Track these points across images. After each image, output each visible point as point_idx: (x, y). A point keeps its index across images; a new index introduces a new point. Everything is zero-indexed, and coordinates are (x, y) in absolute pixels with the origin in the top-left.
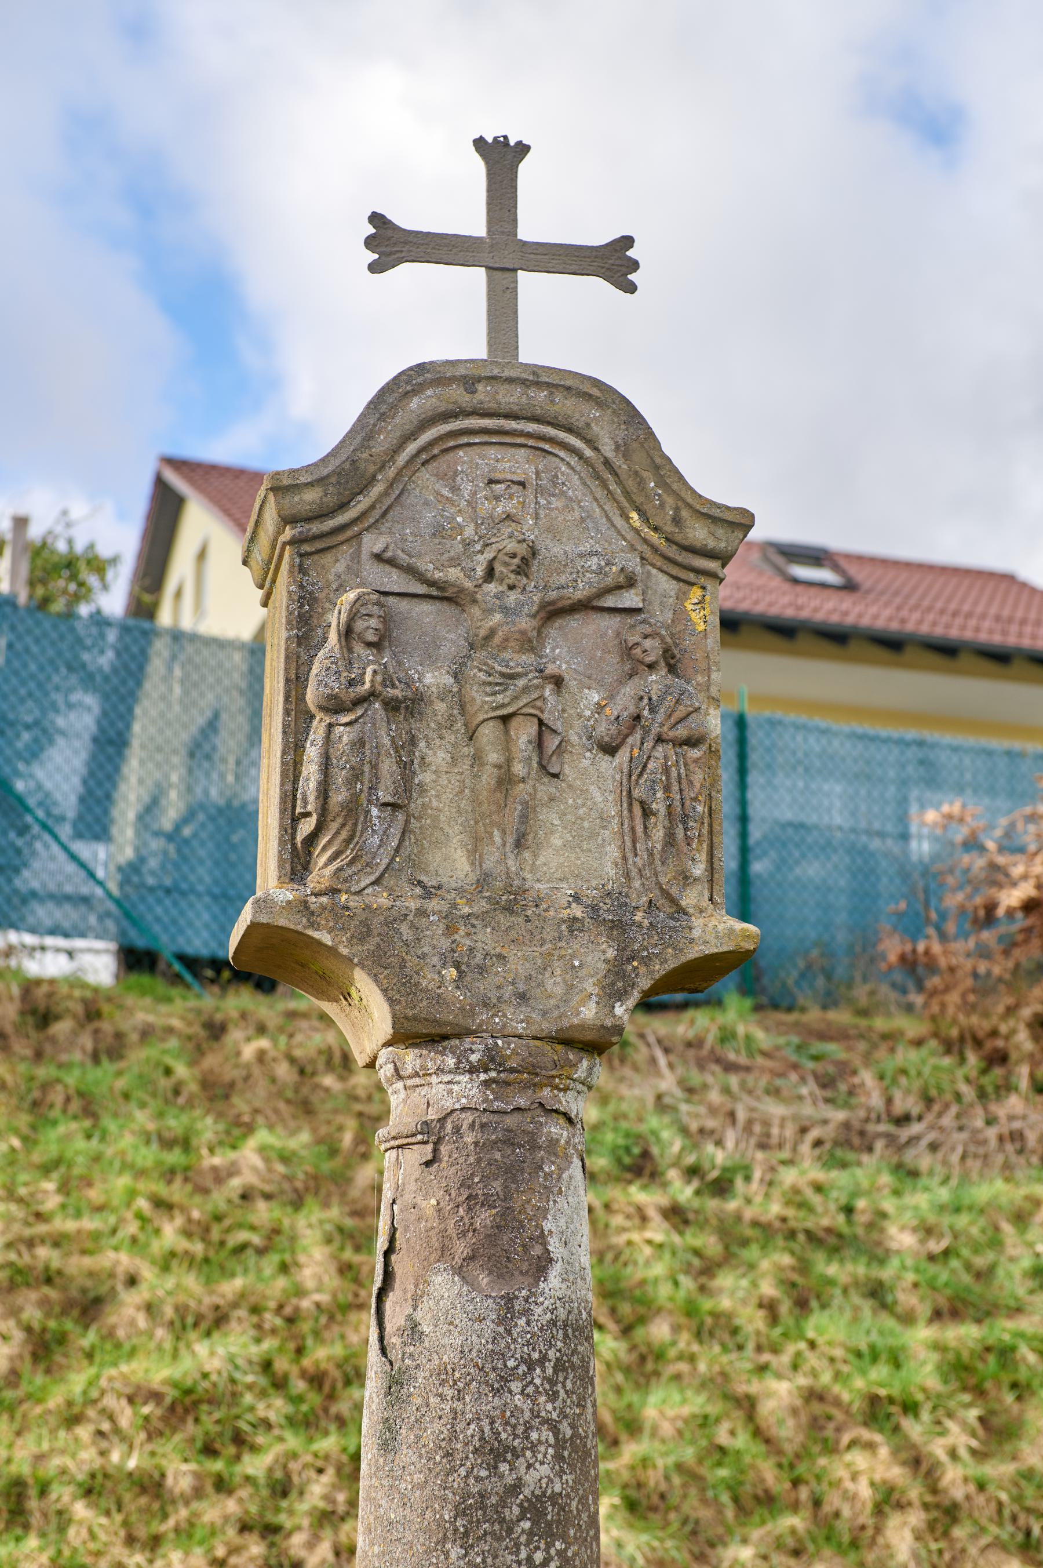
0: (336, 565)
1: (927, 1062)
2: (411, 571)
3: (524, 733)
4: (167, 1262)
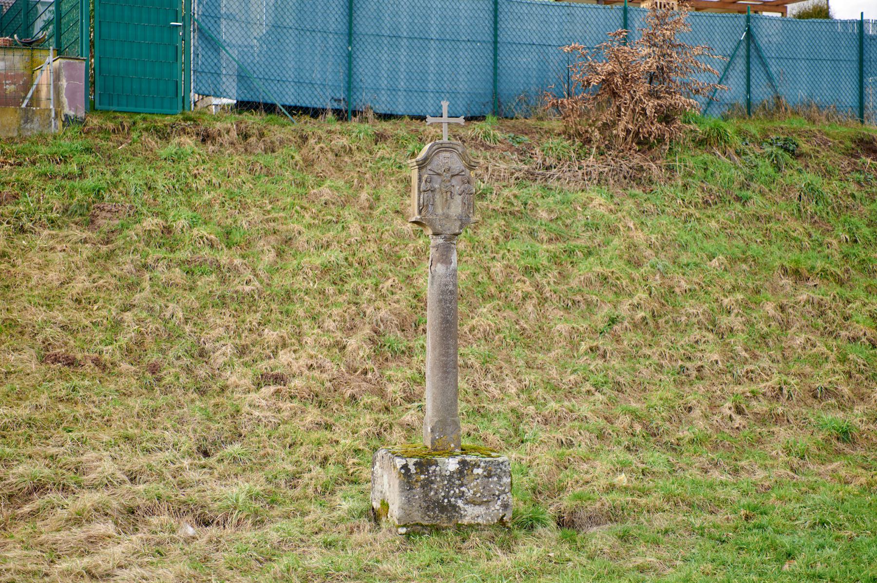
0: (424, 170)
3: (449, 194)
4: (310, 226)
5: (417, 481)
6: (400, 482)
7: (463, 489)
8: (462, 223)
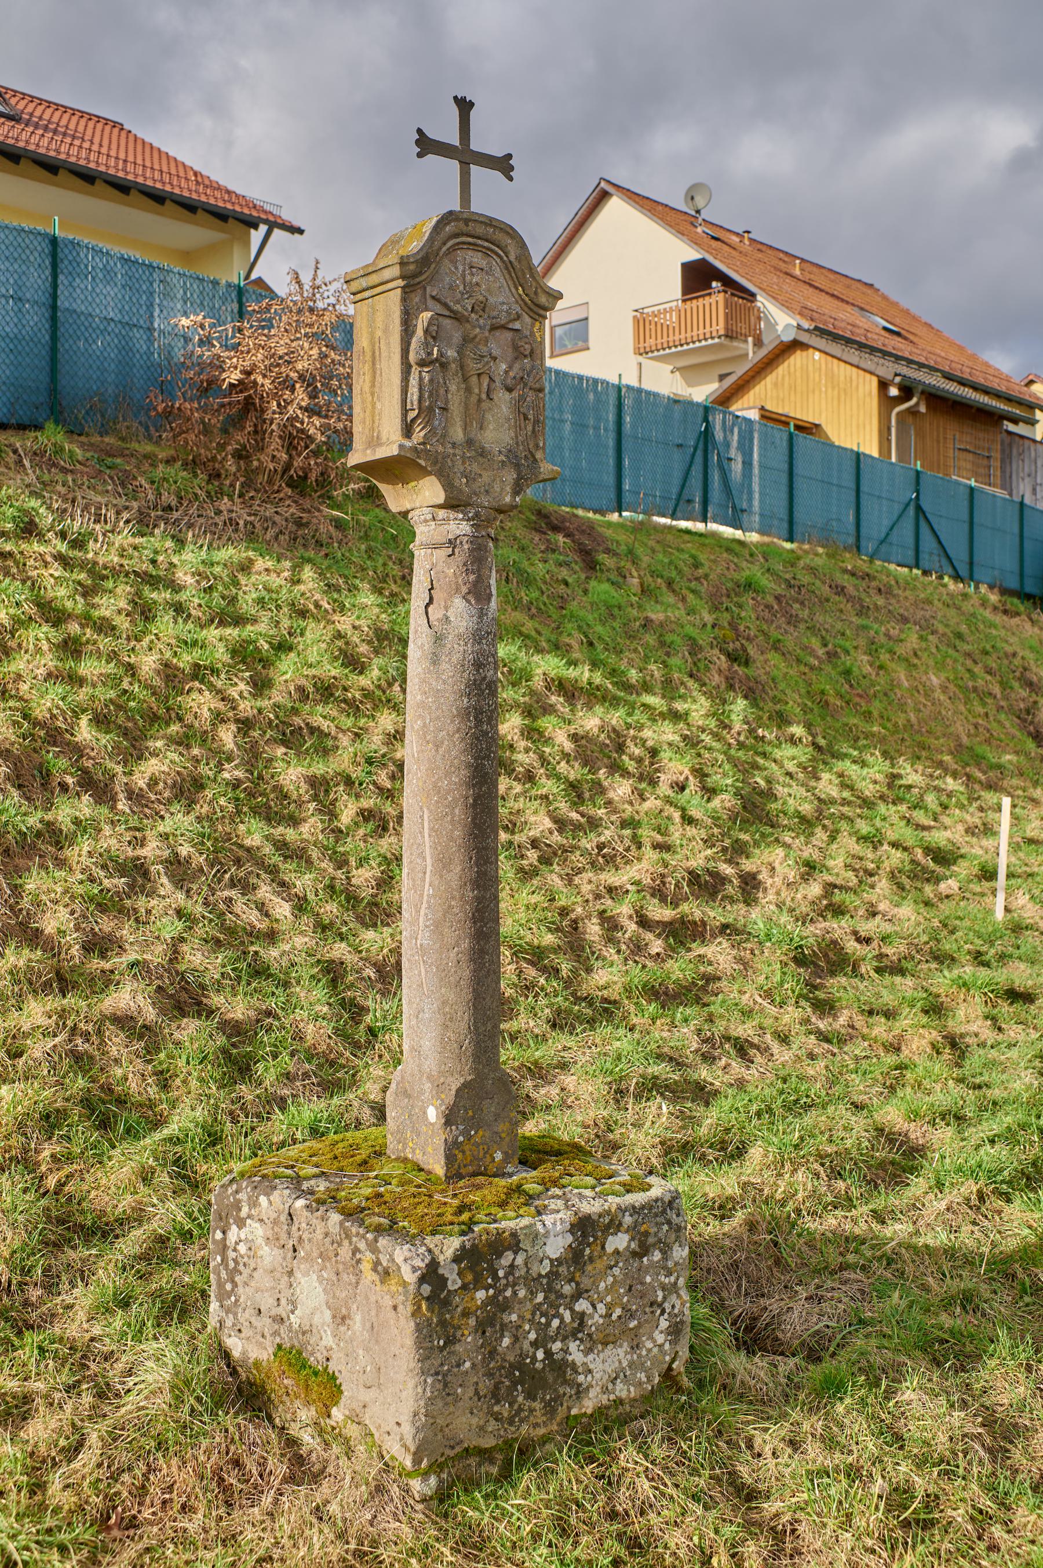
1: (178, 473)
2: (445, 305)
3: (485, 382)
5: (466, 1314)
6: (418, 1328)
7: (582, 1305)
8: (520, 477)
